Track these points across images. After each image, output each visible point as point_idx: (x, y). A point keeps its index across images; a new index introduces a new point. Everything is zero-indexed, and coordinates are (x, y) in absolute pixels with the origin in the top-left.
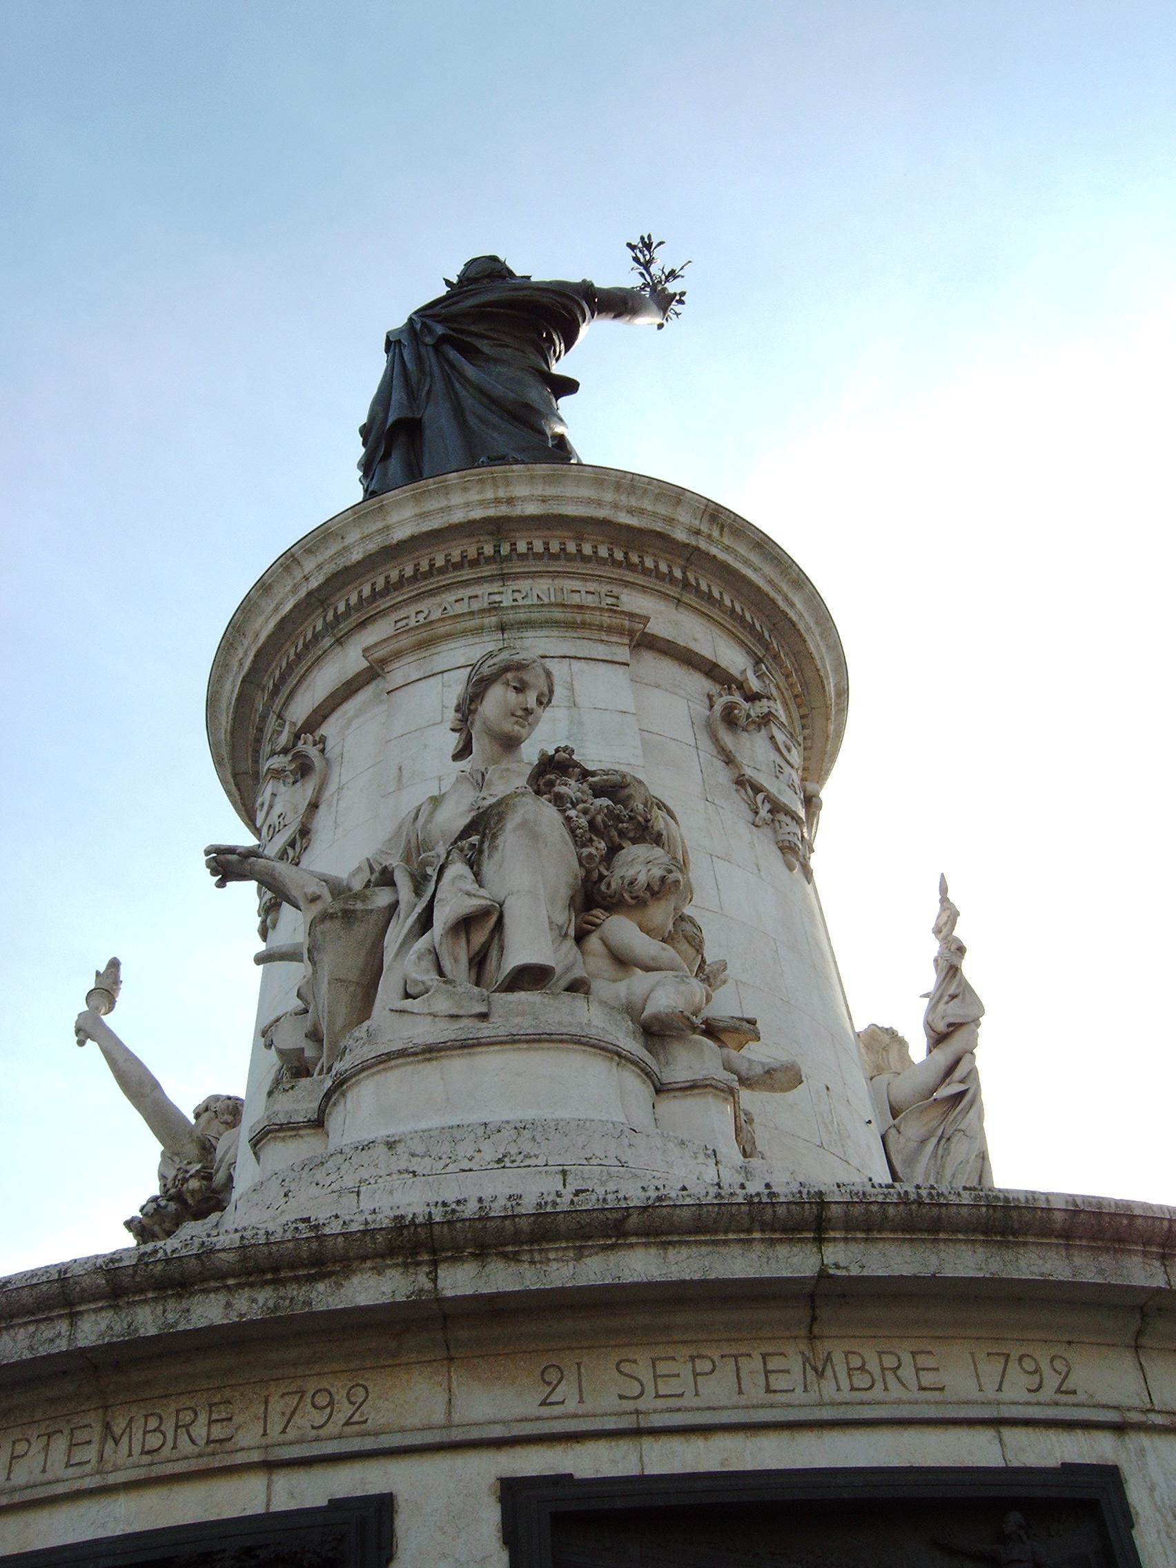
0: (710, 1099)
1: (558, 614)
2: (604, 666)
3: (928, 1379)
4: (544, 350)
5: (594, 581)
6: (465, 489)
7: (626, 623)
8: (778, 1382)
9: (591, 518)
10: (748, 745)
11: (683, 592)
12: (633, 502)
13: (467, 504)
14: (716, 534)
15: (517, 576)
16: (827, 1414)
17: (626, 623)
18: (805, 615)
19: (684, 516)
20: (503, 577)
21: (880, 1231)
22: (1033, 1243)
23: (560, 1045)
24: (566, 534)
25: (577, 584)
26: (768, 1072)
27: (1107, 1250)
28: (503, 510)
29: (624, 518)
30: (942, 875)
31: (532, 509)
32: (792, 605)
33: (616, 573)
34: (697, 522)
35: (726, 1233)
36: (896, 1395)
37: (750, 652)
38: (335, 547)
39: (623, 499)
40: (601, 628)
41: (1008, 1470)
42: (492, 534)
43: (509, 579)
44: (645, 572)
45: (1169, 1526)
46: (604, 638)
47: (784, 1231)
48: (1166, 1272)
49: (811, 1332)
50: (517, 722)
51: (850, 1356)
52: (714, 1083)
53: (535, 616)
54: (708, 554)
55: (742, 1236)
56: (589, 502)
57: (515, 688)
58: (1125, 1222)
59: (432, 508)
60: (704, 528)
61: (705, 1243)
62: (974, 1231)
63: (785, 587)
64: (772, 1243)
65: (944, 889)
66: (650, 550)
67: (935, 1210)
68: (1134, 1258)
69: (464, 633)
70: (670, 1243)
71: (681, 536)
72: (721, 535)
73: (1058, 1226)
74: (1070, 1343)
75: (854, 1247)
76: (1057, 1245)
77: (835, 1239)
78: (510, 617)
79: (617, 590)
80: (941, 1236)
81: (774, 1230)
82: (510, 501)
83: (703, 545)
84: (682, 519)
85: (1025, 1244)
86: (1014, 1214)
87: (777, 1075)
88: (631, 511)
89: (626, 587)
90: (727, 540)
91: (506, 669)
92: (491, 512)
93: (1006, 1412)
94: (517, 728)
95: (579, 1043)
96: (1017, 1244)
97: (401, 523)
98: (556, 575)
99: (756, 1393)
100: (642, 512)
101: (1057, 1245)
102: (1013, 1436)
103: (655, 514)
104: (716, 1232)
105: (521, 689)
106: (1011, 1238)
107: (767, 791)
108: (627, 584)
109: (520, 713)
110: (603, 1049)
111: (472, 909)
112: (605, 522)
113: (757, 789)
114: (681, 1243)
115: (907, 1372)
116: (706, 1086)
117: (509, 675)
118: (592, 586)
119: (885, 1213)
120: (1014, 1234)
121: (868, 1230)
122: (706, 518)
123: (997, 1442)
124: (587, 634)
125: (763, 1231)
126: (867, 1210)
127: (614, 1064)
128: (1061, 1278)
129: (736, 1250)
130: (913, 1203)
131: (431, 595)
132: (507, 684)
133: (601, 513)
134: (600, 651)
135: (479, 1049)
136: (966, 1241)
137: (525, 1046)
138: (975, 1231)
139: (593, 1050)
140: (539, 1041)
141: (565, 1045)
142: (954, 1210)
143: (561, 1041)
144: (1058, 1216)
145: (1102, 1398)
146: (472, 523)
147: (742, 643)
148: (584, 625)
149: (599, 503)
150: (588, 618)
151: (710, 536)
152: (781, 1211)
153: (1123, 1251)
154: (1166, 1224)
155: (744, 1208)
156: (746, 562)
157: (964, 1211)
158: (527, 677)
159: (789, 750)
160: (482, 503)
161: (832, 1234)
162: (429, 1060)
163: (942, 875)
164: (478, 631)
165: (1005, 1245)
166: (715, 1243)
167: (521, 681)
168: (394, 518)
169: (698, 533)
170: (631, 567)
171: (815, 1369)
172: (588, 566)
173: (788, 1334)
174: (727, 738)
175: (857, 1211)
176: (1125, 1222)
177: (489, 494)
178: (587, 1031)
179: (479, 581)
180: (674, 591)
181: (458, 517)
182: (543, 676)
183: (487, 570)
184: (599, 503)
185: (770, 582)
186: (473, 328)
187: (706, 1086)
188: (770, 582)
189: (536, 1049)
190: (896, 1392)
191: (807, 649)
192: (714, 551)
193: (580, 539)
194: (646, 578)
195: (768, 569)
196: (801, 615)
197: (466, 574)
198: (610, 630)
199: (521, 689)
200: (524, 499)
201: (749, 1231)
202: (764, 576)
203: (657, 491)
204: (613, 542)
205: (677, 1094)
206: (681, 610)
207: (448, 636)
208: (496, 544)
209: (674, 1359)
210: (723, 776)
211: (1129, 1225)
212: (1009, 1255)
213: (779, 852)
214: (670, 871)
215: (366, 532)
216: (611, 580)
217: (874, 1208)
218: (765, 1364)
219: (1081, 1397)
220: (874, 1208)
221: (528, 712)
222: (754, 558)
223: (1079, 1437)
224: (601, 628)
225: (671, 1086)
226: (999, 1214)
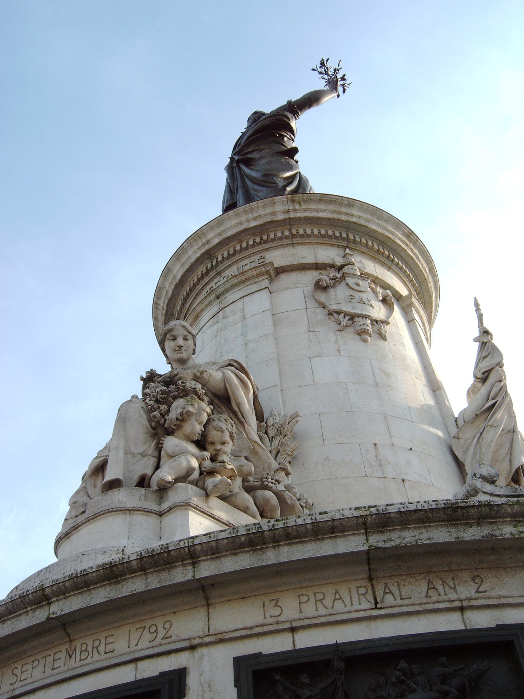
0: (178, 512)
1: (235, 281)
2: (257, 294)
3: (109, 647)
4: (280, 141)
5: (253, 256)
6: (192, 246)
7: (263, 269)
8: (57, 665)
9: (239, 232)
10: (333, 294)
11: (293, 240)
12: (255, 215)
13: (194, 252)
14: (297, 207)
15: (223, 270)
16: (68, 675)
17: (263, 269)
18: (363, 215)
19: (210, 236)
20: (219, 273)
21: (69, 593)
22: (130, 578)
23: (103, 516)
24: (235, 243)
25: (247, 261)
26: (215, 486)
27: (165, 569)
28: (207, 247)
29: (253, 224)
30: (475, 298)
31: (216, 241)
32: (352, 215)
33: (260, 248)
34: (287, 207)
35: (20, 611)
36: (97, 659)
37: (339, 246)
38: (164, 292)
39: (250, 216)
40: (254, 277)
41: (295, 651)
42: (209, 258)
43: (221, 273)
44: (273, 240)
45: (204, 691)
46: (256, 281)
47: (37, 604)
48: (194, 571)
49: (70, 639)
50: (178, 353)
51: (317, 595)
52: (177, 504)
53: (227, 286)
54: (296, 218)
55: (25, 610)
56: (237, 225)
57: (172, 340)
58: (166, 555)
59: (184, 260)
60: (291, 207)
61: (14, 617)
62: (104, 581)
63: (344, 210)
64: (35, 610)
65: (477, 305)
66: (272, 230)
67: (83, 578)
68: (179, 569)
69: (206, 306)
70: (4, 620)
71: (280, 217)
72: (300, 206)
73: (136, 567)
74: (174, 613)
75: (61, 603)
76: (141, 575)
77: (54, 602)
78: (219, 291)
79: (263, 255)
80: (91, 587)
81: (34, 605)
82: (208, 242)
83: (292, 215)
84: (278, 210)
85: (126, 579)
86: (115, 569)
87: (219, 486)
88: (255, 219)
89: (267, 251)
90: (303, 207)
91: (166, 334)
92: (203, 251)
93: (137, 655)
94: (179, 355)
95: (109, 512)
96: (123, 580)
97: (178, 272)
98: (237, 262)
99: (49, 671)
100: (260, 216)
101: (141, 575)
102: (142, 665)
103: (266, 215)
104: (16, 612)
105: (174, 339)
106: (119, 579)
107: (345, 311)
108: (267, 250)
109: (177, 349)
110: (121, 510)
111: (98, 464)
112: (246, 230)
113: (339, 313)
114: (8, 619)
115: (102, 648)
116: (175, 507)
117: (168, 336)
118: (252, 259)
119: (65, 585)
120: (121, 576)
121: (64, 594)
122: (290, 203)
123: (135, 669)
124: (249, 282)
125: (31, 606)
126: (59, 587)
127: (128, 515)
128: (140, 591)
129: (24, 616)
130: (74, 578)
131: (199, 294)
132: (168, 339)
133: (242, 228)
134: (255, 287)
135: (80, 528)
136: (102, 586)
137: (92, 521)
138: (103, 581)
139: (116, 513)
140: (96, 517)
141: (106, 515)
142: (90, 575)
143: (104, 514)
144: (134, 563)
145: (183, 637)
146: (198, 259)
147: (333, 245)
148: (247, 280)
149: (241, 223)
150: (247, 276)
151: (295, 210)
152: (31, 597)
153: (172, 567)
154: (186, 549)
155: (19, 600)
156: (317, 211)
157: (94, 574)
158: (174, 333)
159: (358, 285)
160: (199, 249)
161: (53, 600)
162: (68, 538)
163: (475, 298)
164: (210, 303)
165: (118, 582)
166: (17, 616)
167: (173, 336)
168: (175, 271)
169: (288, 211)
170: (266, 242)
171: (69, 655)
172: (242, 253)
173: (62, 642)
174: (322, 297)
175: (55, 588)
176: (166, 555)
177: (200, 244)
178: (112, 506)
179: (211, 280)
180: (288, 241)
181: (193, 259)
182: (182, 329)
183: (212, 274)
184: (241, 223)
185: (335, 212)
186: (249, 150)
187: (175, 507)
188: (335, 212)
189: (96, 521)
190: (96, 657)
191: (371, 229)
192: (299, 215)
193: (241, 241)
194: (274, 243)
195: (331, 207)
196: (360, 217)
197: (206, 279)
198: (258, 276)
199: (174, 339)
200: (213, 238)
201: (26, 608)
202: (330, 211)
203: (262, 205)
204: (255, 235)
205: (167, 514)
206: (295, 247)
207: (202, 311)
208: (290, 230)
209: (28, 663)
210: (321, 314)
211: (168, 556)
212: (119, 586)
213: (357, 337)
214: (184, 408)
215: (170, 282)
216: (260, 252)
217: (61, 585)
218: (358, 591)
219: (173, 638)
220: (61, 585)
221: (180, 347)
222: (322, 206)
223: (173, 657)
224: (254, 277)
225: (163, 512)
226: (108, 571)
